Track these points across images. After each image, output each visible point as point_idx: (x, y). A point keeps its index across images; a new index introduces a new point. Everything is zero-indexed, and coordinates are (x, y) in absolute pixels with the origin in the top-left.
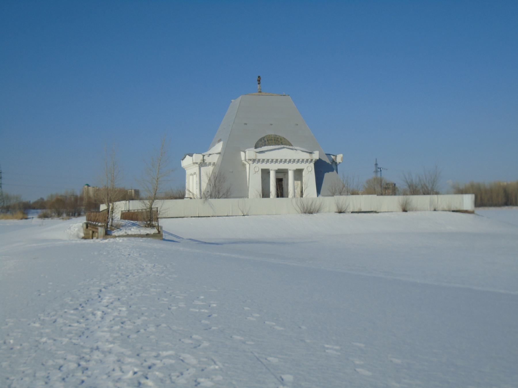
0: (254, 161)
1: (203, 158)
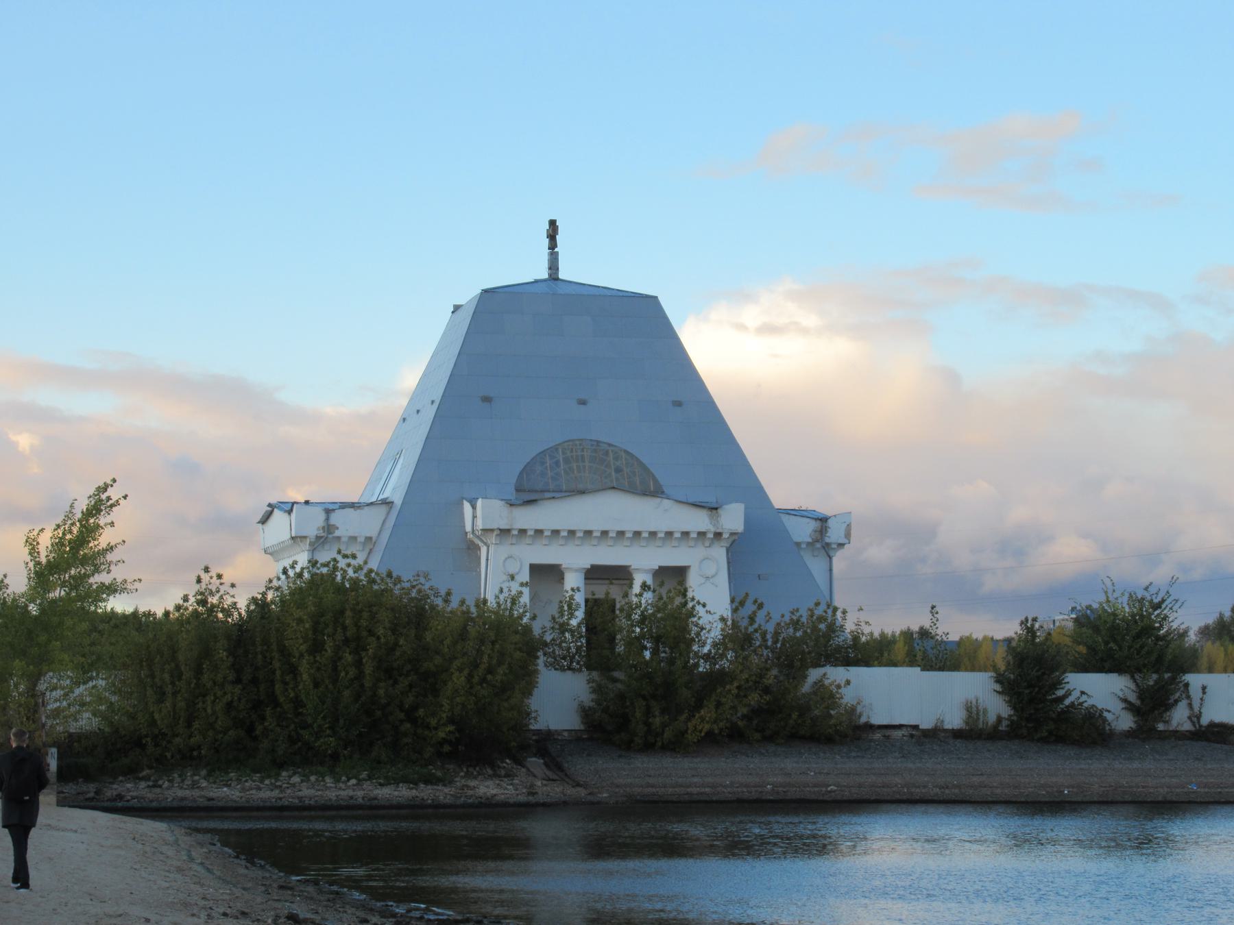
0: (504, 532)
1: (327, 519)
